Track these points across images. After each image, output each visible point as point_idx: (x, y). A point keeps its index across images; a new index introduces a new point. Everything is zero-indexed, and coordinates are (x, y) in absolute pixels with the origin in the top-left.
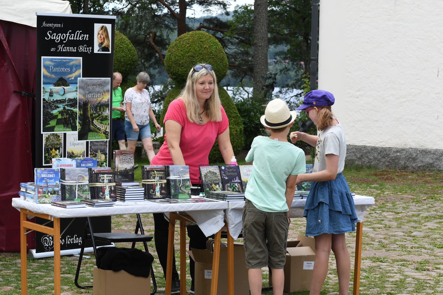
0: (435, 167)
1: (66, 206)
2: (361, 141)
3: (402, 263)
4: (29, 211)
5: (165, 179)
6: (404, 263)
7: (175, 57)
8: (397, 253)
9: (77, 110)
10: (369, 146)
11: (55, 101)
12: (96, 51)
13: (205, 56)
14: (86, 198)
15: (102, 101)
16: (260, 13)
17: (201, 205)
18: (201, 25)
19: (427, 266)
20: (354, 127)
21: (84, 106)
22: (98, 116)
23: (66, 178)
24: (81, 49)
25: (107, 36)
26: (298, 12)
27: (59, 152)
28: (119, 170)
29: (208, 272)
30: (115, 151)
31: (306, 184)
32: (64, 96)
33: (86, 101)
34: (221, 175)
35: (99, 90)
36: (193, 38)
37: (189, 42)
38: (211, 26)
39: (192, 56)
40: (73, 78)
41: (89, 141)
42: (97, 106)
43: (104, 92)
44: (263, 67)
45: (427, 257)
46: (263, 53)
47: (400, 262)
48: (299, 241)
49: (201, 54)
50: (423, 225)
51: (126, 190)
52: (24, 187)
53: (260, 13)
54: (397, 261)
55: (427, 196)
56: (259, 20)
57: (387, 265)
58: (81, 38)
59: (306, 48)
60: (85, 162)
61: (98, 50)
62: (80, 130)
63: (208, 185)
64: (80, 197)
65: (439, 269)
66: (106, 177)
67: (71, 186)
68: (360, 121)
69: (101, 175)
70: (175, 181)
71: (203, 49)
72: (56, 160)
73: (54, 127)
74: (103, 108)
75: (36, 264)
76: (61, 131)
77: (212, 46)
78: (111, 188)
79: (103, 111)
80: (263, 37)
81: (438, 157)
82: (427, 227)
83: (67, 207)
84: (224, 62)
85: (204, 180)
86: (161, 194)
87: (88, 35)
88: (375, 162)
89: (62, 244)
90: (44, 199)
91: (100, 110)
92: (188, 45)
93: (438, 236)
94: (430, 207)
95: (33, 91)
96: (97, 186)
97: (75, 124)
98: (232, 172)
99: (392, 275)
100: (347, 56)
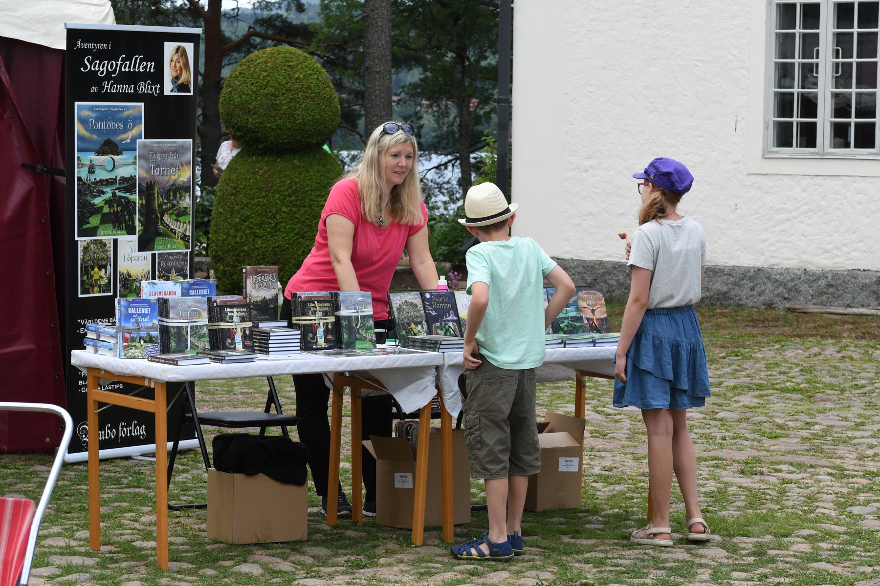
0: (732, 299)
1: (177, 361)
2: (594, 252)
3: (714, 462)
4: (106, 371)
5: (333, 315)
7: (241, 96)
9: (135, 197)
10: (609, 262)
11: (98, 182)
12: (167, 92)
13: (298, 95)
14: (204, 349)
15: (178, 182)
17: (399, 358)
18: (251, 30)
19: (759, 466)
20: (579, 225)
21: (148, 190)
22: (171, 209)
23: (171, 315)
27: (106, 272)
28: (252, 301)
30: (246, 268)
32: (113, 173)
33: (151, 182)
34: (424, 308)
37: (268, 68)
38: (270, 32)
39: (274, 95)
40: (128, 141)
41: (157, 252)
42: (169, 191)
43: (182, 165)
44: (384, 113)
46: (383, 86)
47: (710, 462)
49: (291, 91)
50: (733, 400)
51: (271, 334)
52: (95, 331)
54: (705, 460)
55: (726, 351)
56: (374, 22)
59: (461, 75)
60: (195, 287)
61: (171, 89)
63: (403, 325)
64: (194, 347)
65: (780, 471)
66: (236, 313)
67: (179, 328)
68: (592, 214)
69: (228, 310)
70: (349, 318)
72: (149, 283)
73: (96, 228)
75: (73, 473)
76: (109, 235)
77: (310, 74)
78: (245, 330)
79: (180, 198)
80: (382, 56)
82: (741, 404)
83: (180, 363)
84: (333, 106)
85: (396, 316)
86: (326, 341)
87: (153, 63)
88: (620, 292)
89: (113, 437)
90: (133, 351)
91: (175, 196)
92: (265, 74)
93: (764, 419)
94: (736, 370)
96: (222, 327)
97: (133, 222)
98: (443, 302)
100: (566, 94)
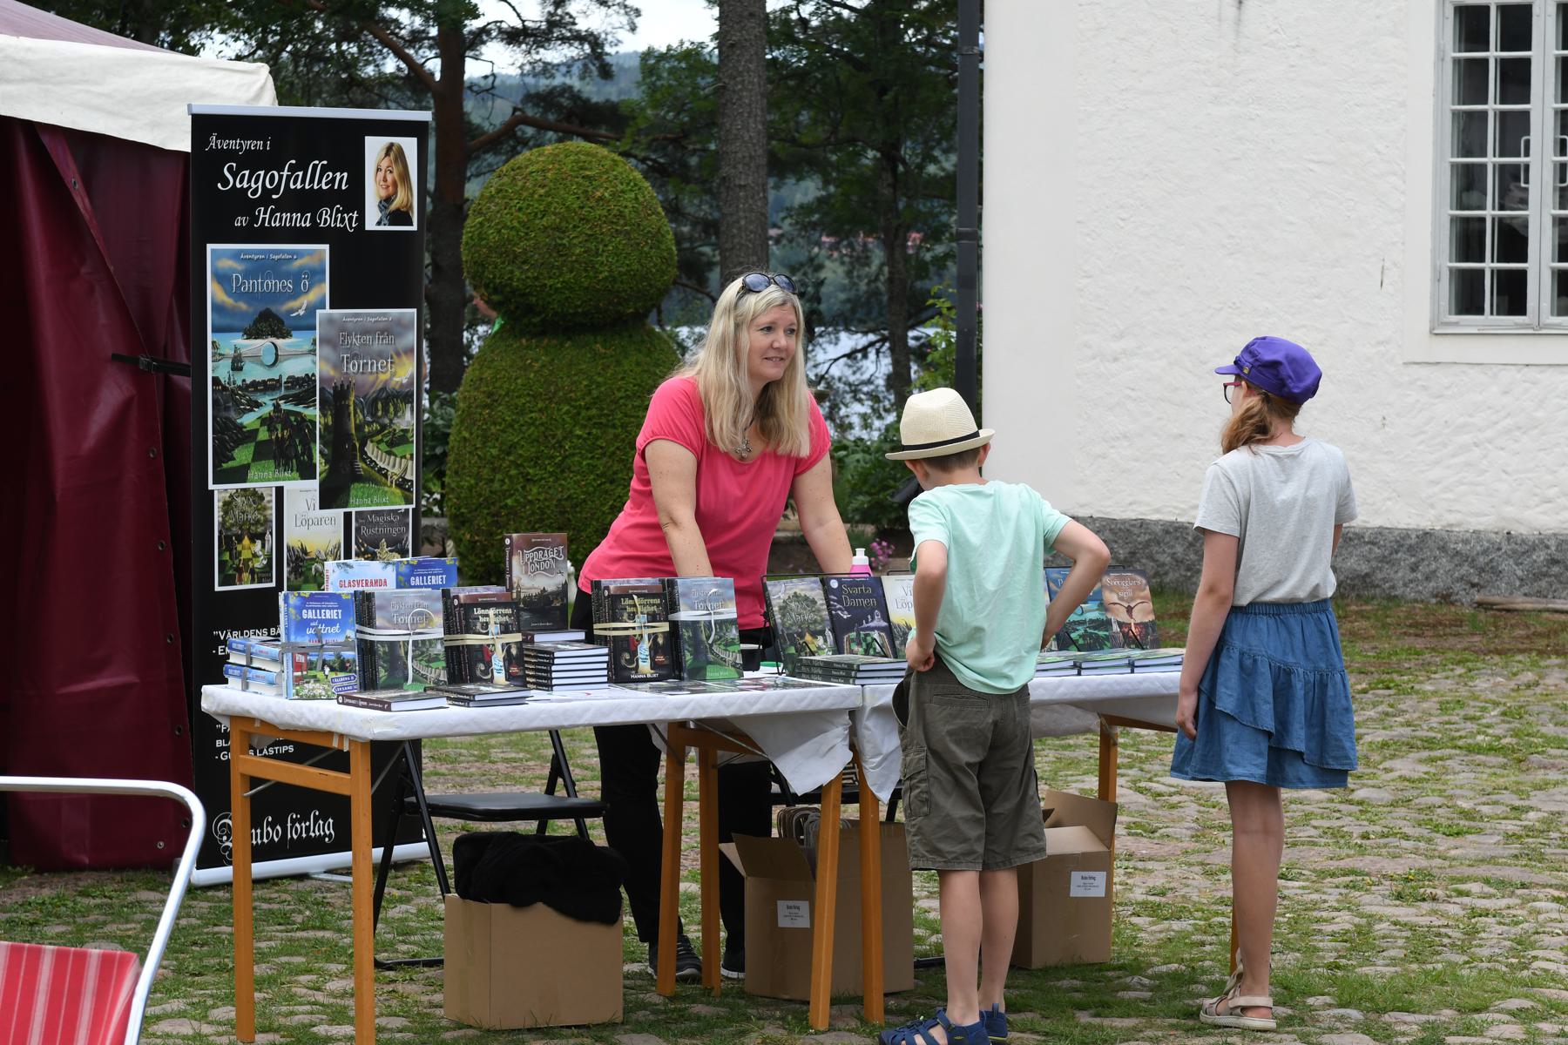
0: (1377, 586)
1: (389, 704)
2: (1131, 504)
3: (1347, 879)
4: (263, 722)
5: (666, 620)
6: (1356, 880)
7: (499, 232)
8: (1327, 851)
9: (314, 413)
10: (1157, 522)
11: (248, 386)
12: (371, 225)
13: (601, 228)
16: (740, 74)
17: (785, 695)
18: (518, 113)
19: (1429, 886)
20: (1104, 456)
21: (336, 399)
22: (378, 432)
23: (379, 622)
24: (326, 220)
25: (405, 176)
26: (860, 66)
27: (263, 546)
29: (789, 907)
30: (510, 538)
31: (1081, 630)
33: (342, 385)
34: (829, 605)
35: (381, 347)
36: (557, 166)
37: (547, 182)
38: (551, 117)
39: (558, 229)
40: (301, 312)
41: (353, 510)
42: (375, 401)
43: (398, 354)
45: (1423, 862)
46: (752, 210)
48: (1052, 810)
49: (588, 221)
50: (1381, 767)
51: (556, 655)
52: (243, 651)
53: (740, 74)
54: (1333, 875)
55: (1368, 679)
57: (1303, 888)
58: (327, 184)
59: (891, 190)
60: (421, 571)
62: (324, 475)
65: (1468, 894)
67: (392, 645)
68: (1125, 437)
71: (594, 204)
72: (338, 565)
73: (246, 468)
74: (394, 405)
76: (269, 480)
77: (623, 192)
78: (509, 648)
79: (396, 414)
80: (751, 157)
81: (1387, 553)
83: (394, 706)
84: (663, 247)
85: (779, 621)
86: (654, 665)
87: (345, 174)
88: (1177, 575)
90: (311, 686)
91: (386, 411)
92: (542, 191)
93: (1437, 800)
94: (1387, 714)
95: (165, 355)
96: (469, 642)
97: (311, 457)
98: (862, 595)
99: (1324, 914)
